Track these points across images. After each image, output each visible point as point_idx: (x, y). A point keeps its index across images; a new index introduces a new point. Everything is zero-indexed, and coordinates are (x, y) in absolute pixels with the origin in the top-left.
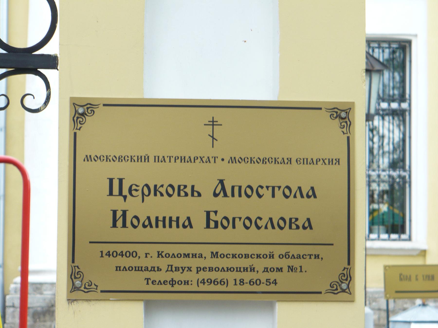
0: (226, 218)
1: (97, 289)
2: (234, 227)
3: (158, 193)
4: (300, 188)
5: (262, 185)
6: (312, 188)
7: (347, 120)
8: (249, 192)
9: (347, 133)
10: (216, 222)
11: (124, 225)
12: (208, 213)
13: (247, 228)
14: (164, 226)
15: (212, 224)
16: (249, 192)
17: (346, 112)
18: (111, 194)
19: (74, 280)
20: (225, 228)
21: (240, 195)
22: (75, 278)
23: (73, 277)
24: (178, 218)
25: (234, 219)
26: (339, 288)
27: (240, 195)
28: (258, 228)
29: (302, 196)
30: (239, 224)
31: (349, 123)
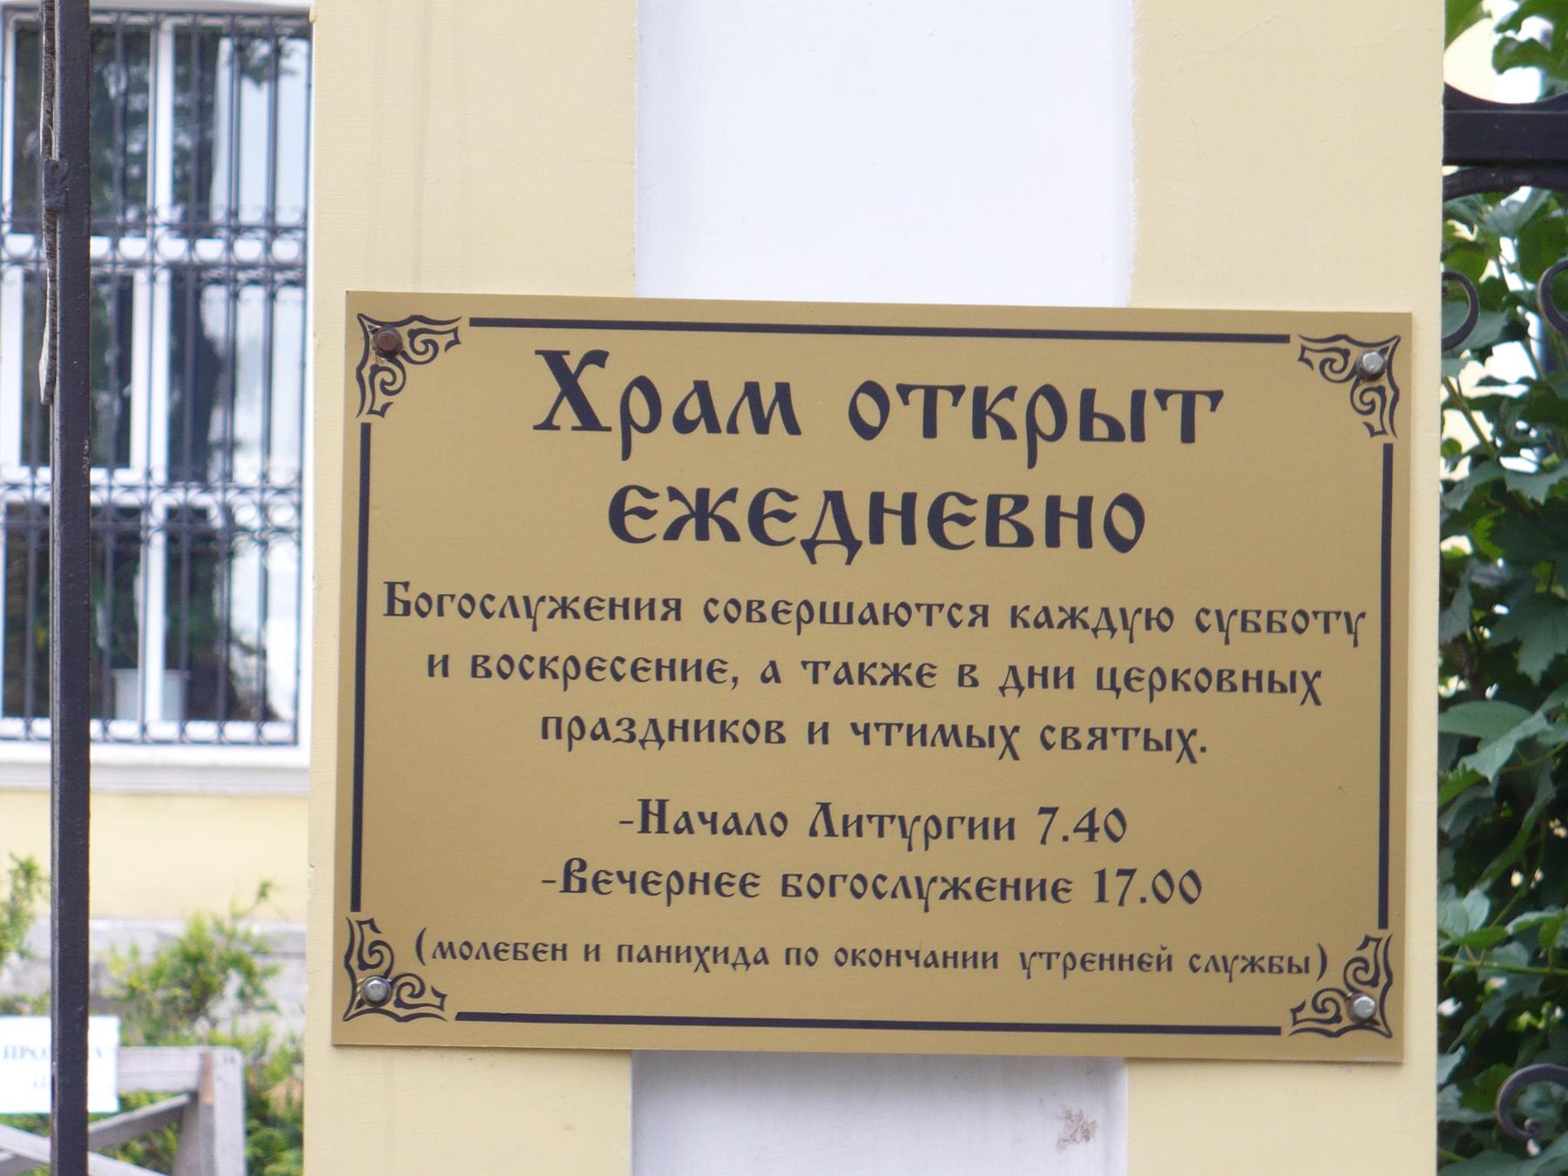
0: (425, 596)
1: (441, 1007)
7: (1384, 381)
9: (1384, 432)
10: (407, 604)
15: (399, 608)
17: (1383, 352)
19: (361, 977)
20: (423, 614)
22: (363, 966)
23: (354, 963)
25: (441, 598)
26: (1343, 1012)
30: (450, 607)
31: (1390, 394)
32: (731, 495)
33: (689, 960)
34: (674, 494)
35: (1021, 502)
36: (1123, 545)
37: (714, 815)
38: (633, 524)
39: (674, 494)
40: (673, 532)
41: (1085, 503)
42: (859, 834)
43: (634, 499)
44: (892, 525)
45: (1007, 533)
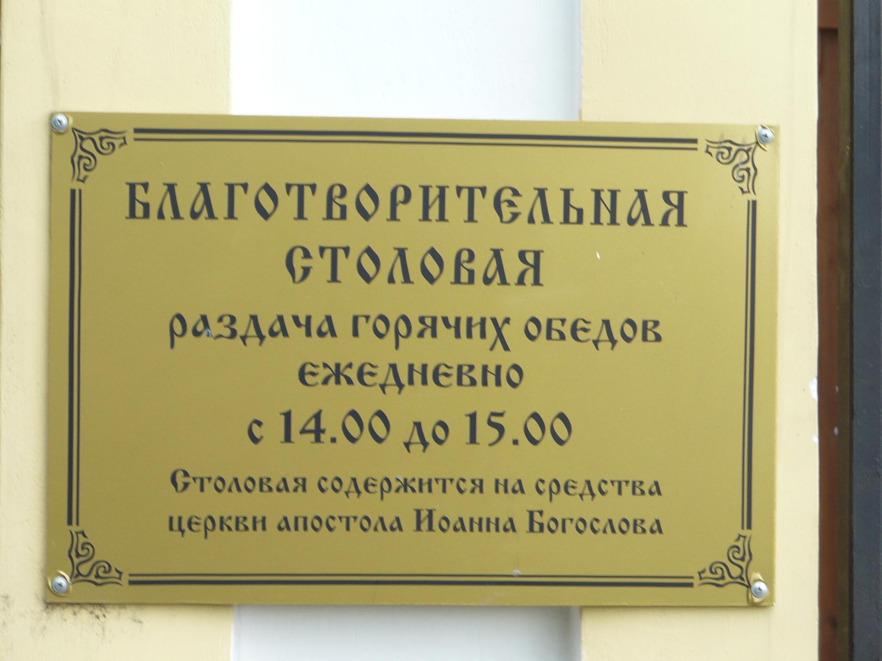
2: (564, 530)
3: (225, 527)
4: (381, 519)
5: (543, 478)
6: (398, 519)
8: (317, 524)
10: (541, 525)
11: (430, 528)
12: (531, 514)
13: (580, 531)
14: (480, 530)
15: (536, 527)
16: (317, 524)
18: (171, 529)
21: (305, 528)
24: (497, 520)
25: (564, 521)
27: (305, 528)
28: (594, 531)
29: (384, 529)
30: (570, 527)
32: (350, 366)
33: (483, 335)
34: (326, 366)
35: (471, 368)
36: (514, 385)
37: (308, 319)
38: (309, 379)
39: (326, 366)
40: (326, 381)
41: (498, 368)
42: (430, 490)
43: (309, 368)
44: (417, 377)
45: (466, 380)
